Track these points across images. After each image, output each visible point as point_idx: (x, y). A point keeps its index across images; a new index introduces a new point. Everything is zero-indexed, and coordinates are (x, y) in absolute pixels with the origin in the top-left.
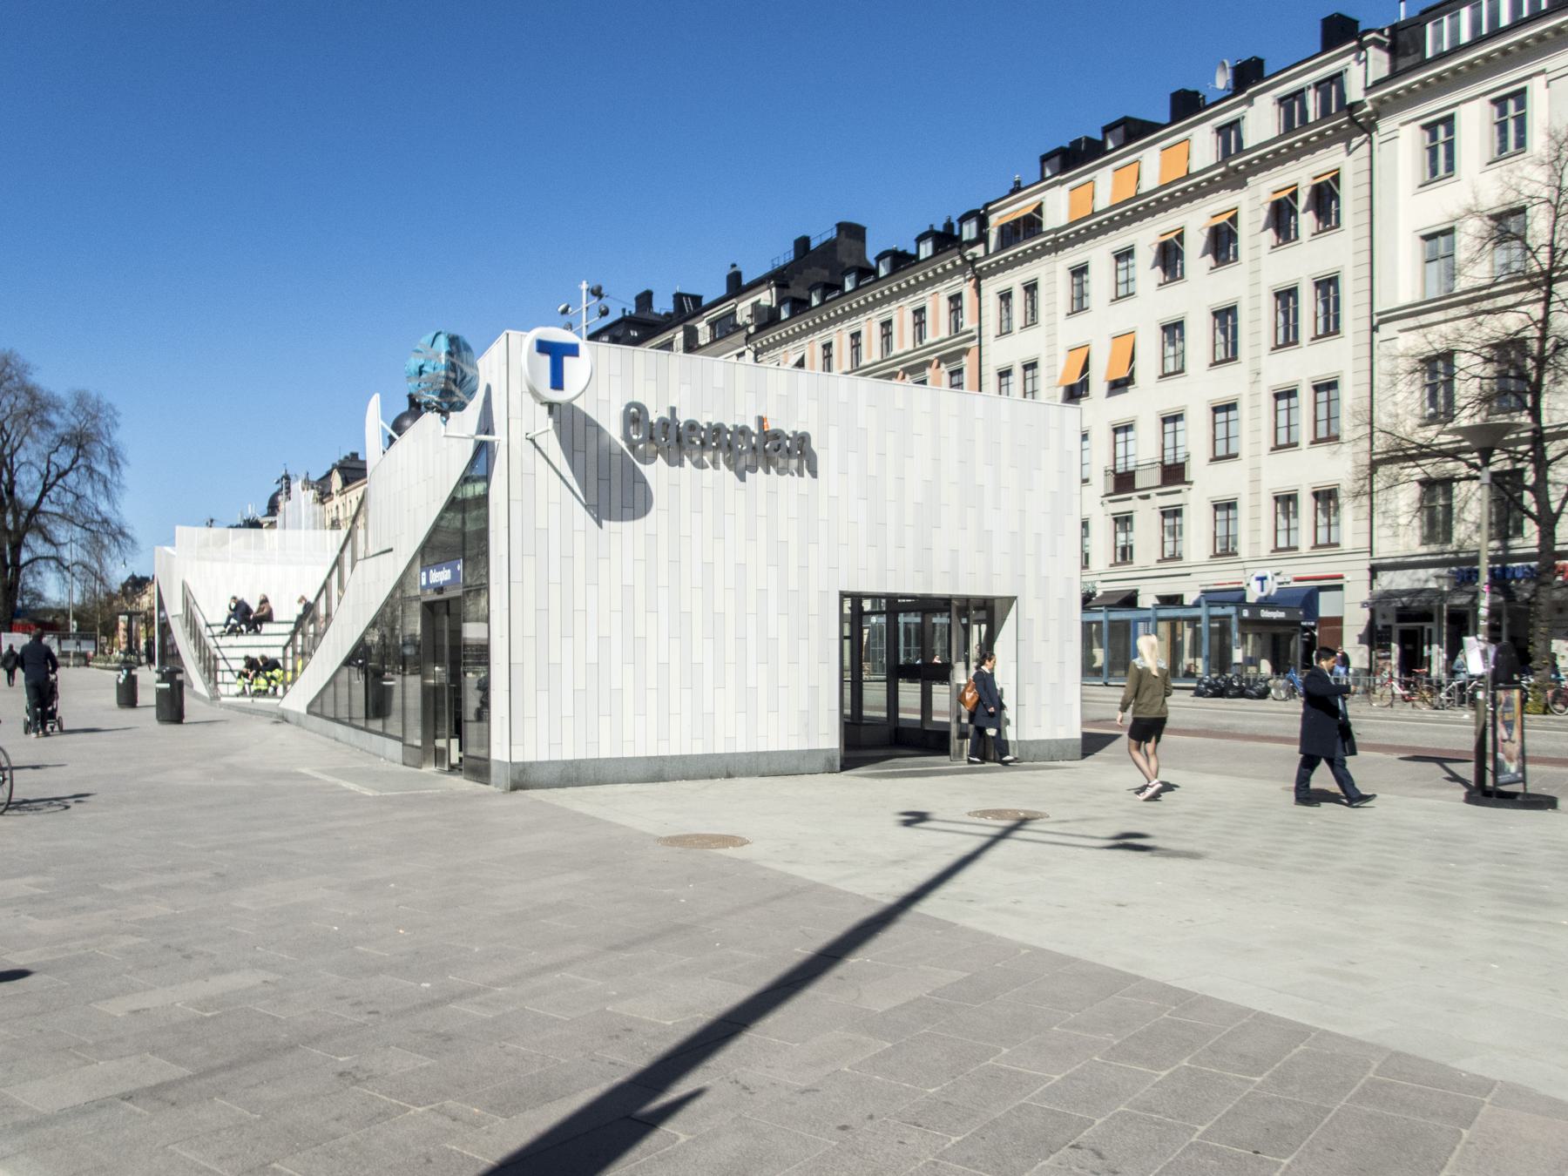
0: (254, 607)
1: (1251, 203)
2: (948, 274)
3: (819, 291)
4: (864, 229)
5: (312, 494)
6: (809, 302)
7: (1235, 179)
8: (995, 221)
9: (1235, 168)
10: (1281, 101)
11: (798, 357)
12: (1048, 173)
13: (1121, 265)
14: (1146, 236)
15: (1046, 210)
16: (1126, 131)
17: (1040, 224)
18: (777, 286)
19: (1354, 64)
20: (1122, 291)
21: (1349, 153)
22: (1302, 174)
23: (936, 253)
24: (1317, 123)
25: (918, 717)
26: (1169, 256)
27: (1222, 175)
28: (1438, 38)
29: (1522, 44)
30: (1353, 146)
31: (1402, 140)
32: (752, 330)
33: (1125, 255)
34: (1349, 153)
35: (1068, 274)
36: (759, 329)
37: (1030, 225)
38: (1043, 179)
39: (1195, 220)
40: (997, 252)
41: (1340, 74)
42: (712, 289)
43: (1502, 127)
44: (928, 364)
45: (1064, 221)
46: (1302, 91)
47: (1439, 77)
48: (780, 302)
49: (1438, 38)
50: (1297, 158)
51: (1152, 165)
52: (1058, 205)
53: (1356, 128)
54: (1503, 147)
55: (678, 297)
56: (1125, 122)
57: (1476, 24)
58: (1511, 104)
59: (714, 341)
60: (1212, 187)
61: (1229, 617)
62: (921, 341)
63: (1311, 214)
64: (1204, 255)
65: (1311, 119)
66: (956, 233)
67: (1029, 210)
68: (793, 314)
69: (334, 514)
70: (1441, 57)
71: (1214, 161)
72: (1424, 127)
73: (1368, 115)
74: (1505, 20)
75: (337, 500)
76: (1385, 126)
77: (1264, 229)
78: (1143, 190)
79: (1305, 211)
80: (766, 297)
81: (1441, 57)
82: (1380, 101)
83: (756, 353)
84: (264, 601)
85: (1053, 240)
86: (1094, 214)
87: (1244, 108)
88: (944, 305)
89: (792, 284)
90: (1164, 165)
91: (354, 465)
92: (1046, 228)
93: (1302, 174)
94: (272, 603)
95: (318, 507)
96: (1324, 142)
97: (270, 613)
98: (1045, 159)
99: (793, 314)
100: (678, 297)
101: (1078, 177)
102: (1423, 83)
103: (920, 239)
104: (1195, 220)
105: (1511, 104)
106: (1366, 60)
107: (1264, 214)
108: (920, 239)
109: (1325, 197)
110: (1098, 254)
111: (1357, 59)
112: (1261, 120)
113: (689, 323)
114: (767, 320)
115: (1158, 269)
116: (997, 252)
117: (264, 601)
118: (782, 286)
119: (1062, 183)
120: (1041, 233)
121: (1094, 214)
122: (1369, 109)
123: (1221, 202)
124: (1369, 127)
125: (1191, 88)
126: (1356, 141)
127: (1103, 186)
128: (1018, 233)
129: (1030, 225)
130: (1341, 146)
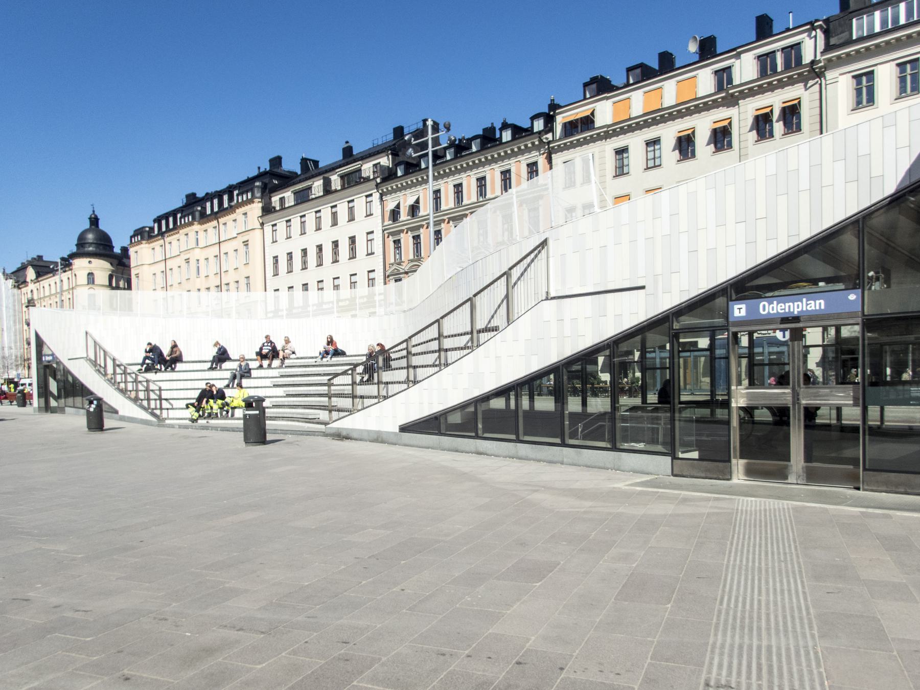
0: (166, 351)
1: (741, 118)
2: (528, 150)
3: (402, 167)
5: (10, 282)
6: (396, 173)
7: (732, 101)
8: (560, 120)
9: (732, 95)
10: (716, 72)
11: (396, 203)
12: (588, 96)
13: (649, 149)
14: (669, 133)
15: (597, 114)
16: (642, 72)
17: (593, 122)
18: (392, 154)
19: (807, 39)
20: (651, 164)
21: (806, 90)
22: (776, 100)
23: (514, 138)
24: (782, 73)
26: (685, 145)
27: (722, 98)
28: (860, 27)
29: (888, 43)
30: (809, 85)
31: (840, 84)
32: (378, 180)
33: (653, 143)
34: (806, 90)
35: (613, 152)
36: (384, 180)
37: (587, 122)
38: (585, 99)
39: (702, 125)
40: (560, 139)
41: (730, 67)
42: (328, 155)
43: (859, 92)
44: (402, 231)
45: (609, 122)
46: (774, 52)
47: (867, 49)
48: (396, 165)
49: (860, 27)
50: (772, 91)
51: (669, 91)
52: (605, 111)
53: (814, 74)
54: (859, 102)
55: (304, 161)
56: (641, 66)
57: (884, 22)
58: (864, 79)
59: (343, 188)
60: (716, 105)
62: (437, 210)
63: (781, 123)
64: (708, 144)
65: (779, 69)
66: (498, 136)
67: (588, 113)
68: (406, 173)
69: (30, 296)
70: (861, 39)
71: (756, 77)
72: (854, 77)
73: (821, 68)
74: (902, 21)
75: (31, 286)
76: (830, 75)
77: (750, 131)
78: (665, 106)
79: (777, 121)
80: (385, 161)
81: (861, 39)
82: (829, 60)
83: (381, 195)
84: (175, 346)
85: (605, 132)
86: (630, 119)
87: (733, 60)
88: (430, 196)
89: (400, 153)
90: (646, 102)
91: (41, 264)
92: (597, 125)
93: (776, 100)
94: (181, 346)
95: (16, 291)
96: (791, 82)
97: (181, 355)
98: (586, 85)
99: (406, 173)
100: (304, 161)
101: (651, 85)
102: (858, 51)
103: (534, 118)
104: (702, 125)
105: (864, 79)
106: (815, 37)
107: (750, 121)
108: (534, 118)
109: (791, 114)
110: (635, 142)
111: (809, 36)
112: (745, 68)
113: (326, 175)
114: (388, 176)
115: (677, 152)
116: (560, 139)
117: (175, 346)
118: (395, 154)
119: (608, 98)
120: (594, 129)
121: (630, 119)
122: (822, 64)
123: (720, 114)
124: (820, 75)
125: (772, 17)
126: (811, 83)
127: (638, 101)
128: (576, 127)
129: (587, 122)
130: (801, 85)
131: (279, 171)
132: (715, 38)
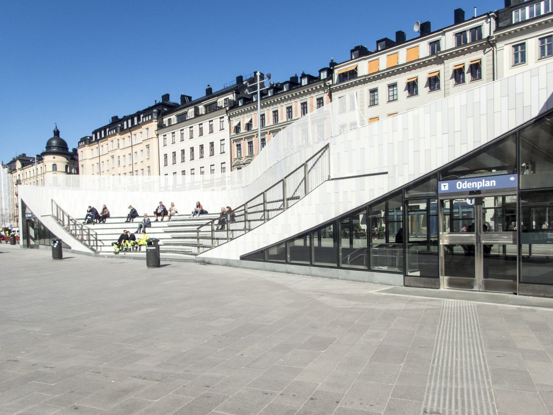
0: (100, 211)
1: (445, 71)
2: (317, 90)
3: (242, 100)
4: (430, 23)
5: (6, 170)
6: (238, 104)
7: (440, 61)
8: (337, 72)
9: (440, 57)
10: (430, 43)
11: (238, 122)
12: (353, 58)
13: (390, 90)
14: (402, 80)
15: (359, 68)
16: (386, 43)
17: (356, 73)
18: (236, 93)
19: (485, 23)
20: (391, 98)
21: (485, 54)
22: (466, 60)
23: (309, 83)
24: (470, 44)
25: (426, 239)
26: (412, 87)
27: (434, 59)
28: (517, 16)
29: (534, 26)
30: (486, 51)
31: (505, 51)
32: (227, 108)
33: (393, 86)
34: (485, 54)
35: (369, 92)
36: (231, 108)
37: (353, 73)
38: (352, 59)
39: (422, 75)
40: (337, 84)
41: (439, 40)
42: (197, 93)
43: (516, 55)
44: (242, 139)
45: (366, 73)
46: (465, 31)
47: (521, 29)
48: (238, 99)
49: (517, 16)
50: (464, 54)
51: (402, 55)
52: (363, 67)
53: (489, 45)
54: (516, 62)
55: (183, 97)
56: (386, 40)
57: (531, 13)
58: (519, 47)
59: (206, 113)
60: (430, 63)
61: (470, 212)
62: (263, 126)
63: (470, 74)
64: (426, 87)
65: (468, 42)
66: (299, 82)
67: (354, 68)
68: (244, 104)
69: (18, 178)
70: (518, 24)
71: (454, 47)
72: (513, 46)
73: (493, 41)
74: (542, 13)
75: (19, 172)
76: (499, 45)
77: (451, 79)
78: (400, 63)
79: (467, 73)
80: (231, 97)
81: (518, 24)
82: (499, 36)
83: (229, 117)
84: (105, 208)
85: (363, 79)
86: (379, 72)
87: (441, 36)
88: (259, 118)
89: (240, 92)
90: (388, 62)
91: (25, 159)
92: (359, 75)
93: (466, 60)
94: (109, 208)
95: (9, 175)
96: (476, 49)
97: (109, 214)
98: (352, 51)
99: (244, 104)
100: (183, 97)
101: (392, 51)
102: (515, 31)
103: (321, 71)
104: (422, 75)
105: (519, 47)
106: (490, 22)
107: (451, 73)
108: (321, 71)
109: (476, 69)
110: (382, 85)
111: (486, 21)
112: (448, 41)
113: (196, 105)
114: (233, 106)
115: (407, 91)
116: (337, 84)
117: (105, 208)
118: (237, 93)
119: (365, 59)
120: (357, 77)
121: (379, 72)
122: (494, 39)
123: (433, 69)
124: (493, 45)
126: (487, 50)
127: (383, 61)
128: (346, 76)
129: (353, 73)
130: (482, 51)
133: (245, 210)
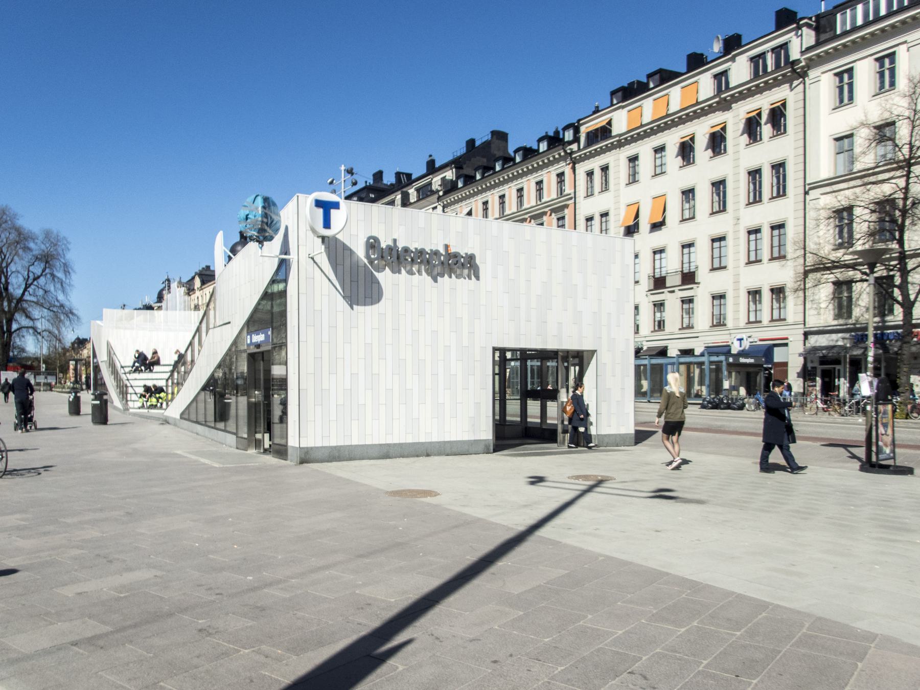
0: (149, 356)
1: (734, 119)
2: (556, 161)
3: (480, 171)
5: (183, 290)
6: (474, 177)
7: (724, 105)
8: (584, 130)
9: (725, 99)
10: (752, 59)
11: (468, 209)
12: (615, 102)
13: (658, 156)
14: (672, 139)
15: (614, 123)
16: (661, 77)
17: (610, 131)
18: (456, 168)
19: (795, 37)
20: (658, 171)
21: (792, 90)
22: (764, 102)
23: (549, 148)
24: (773, 72)
25: (539, 421)
26: (686, 150)
27: (717, 102)
28: (844, 23)
29: (893, 26)
30: (794, 85)
31: (822, 82)
32: (441, 193)
33: (660, 150)
34: (792, 90)
35: (627, 161)
36: (446, 193)
37: (605, 132)
38: (612, 105)
39: (701, 129)
40: (585, 148)
41: (786, 44)
42: (418, 170)
43: (881, 75)
44: (545, 213)
45: (624, 130)
46: (764, 53)
47: (844, 45)
48: (458, 177)
49: (844, 23)
50: (761, 93)
51: (676, 97)
52: (621, 120)
53: (796, 75)
54: (882, 86)
55: (398, 174)
56: (660, 71)
57: (866, 14)
58: (887, 61)
59: (419, 200)
60: (711, 110)
62: (540, 200)
63: (769, 125)
64: (706, 150)
65: (769, 70)
66: (561, 136)
67: (604, 123)
68: (465, 184)
69: (196, 302)
70: (845, 33)
71: (712, 95)
72: (836, 75)
73: (803, 67)
74: (883, 12)
75: (198, 293)
76: (812, 74)
77: (742, 135)
78: (670, 112)
79: (766, 124)
80: (450, 174)
81: (845, 33)
82: (810, 59)
83: (444, 207)
84: (155, 353)
85: (618, 141)
86: (642, 126)
87: (730, 63)
88: (554, 179)
89: (464, 166)
90: (683, 97)
91: (208, 273)
92: (614, 134)
93: (764, 102)
94: (160, 354)
95: (187, 297)
96: (777, 83)
97: (159, 360)
98: (613, 93)
99: (465, 184)
100: (398, 174)
101: (633, 104)
102: (835, 49)
103: (540, 140)
104: (701, 129)
105: (887, 61)
106: (801, 35)
107: (741, 126)
108: (540, 140)
109: (777, 116)
110: (644, 149)
111: (796, 34)
112: (740, 70)
113: (404, 190)
114: (450, 188)
115: (680, 158)
116: (585, 148)
117: (155, 353)
118: (459, 168)
119: (623, 107)
120: (611, 137)
121: (642, 126)
122: (803, 64)
123: (716, 119)
124: (803, 75)
126: (795, 83)
127: (647, 109)
128: (597, 137)
129: (605, 132)
130: (787, 86)
131: (382, 186)
132: (507, 134)
133: (77, 361)
